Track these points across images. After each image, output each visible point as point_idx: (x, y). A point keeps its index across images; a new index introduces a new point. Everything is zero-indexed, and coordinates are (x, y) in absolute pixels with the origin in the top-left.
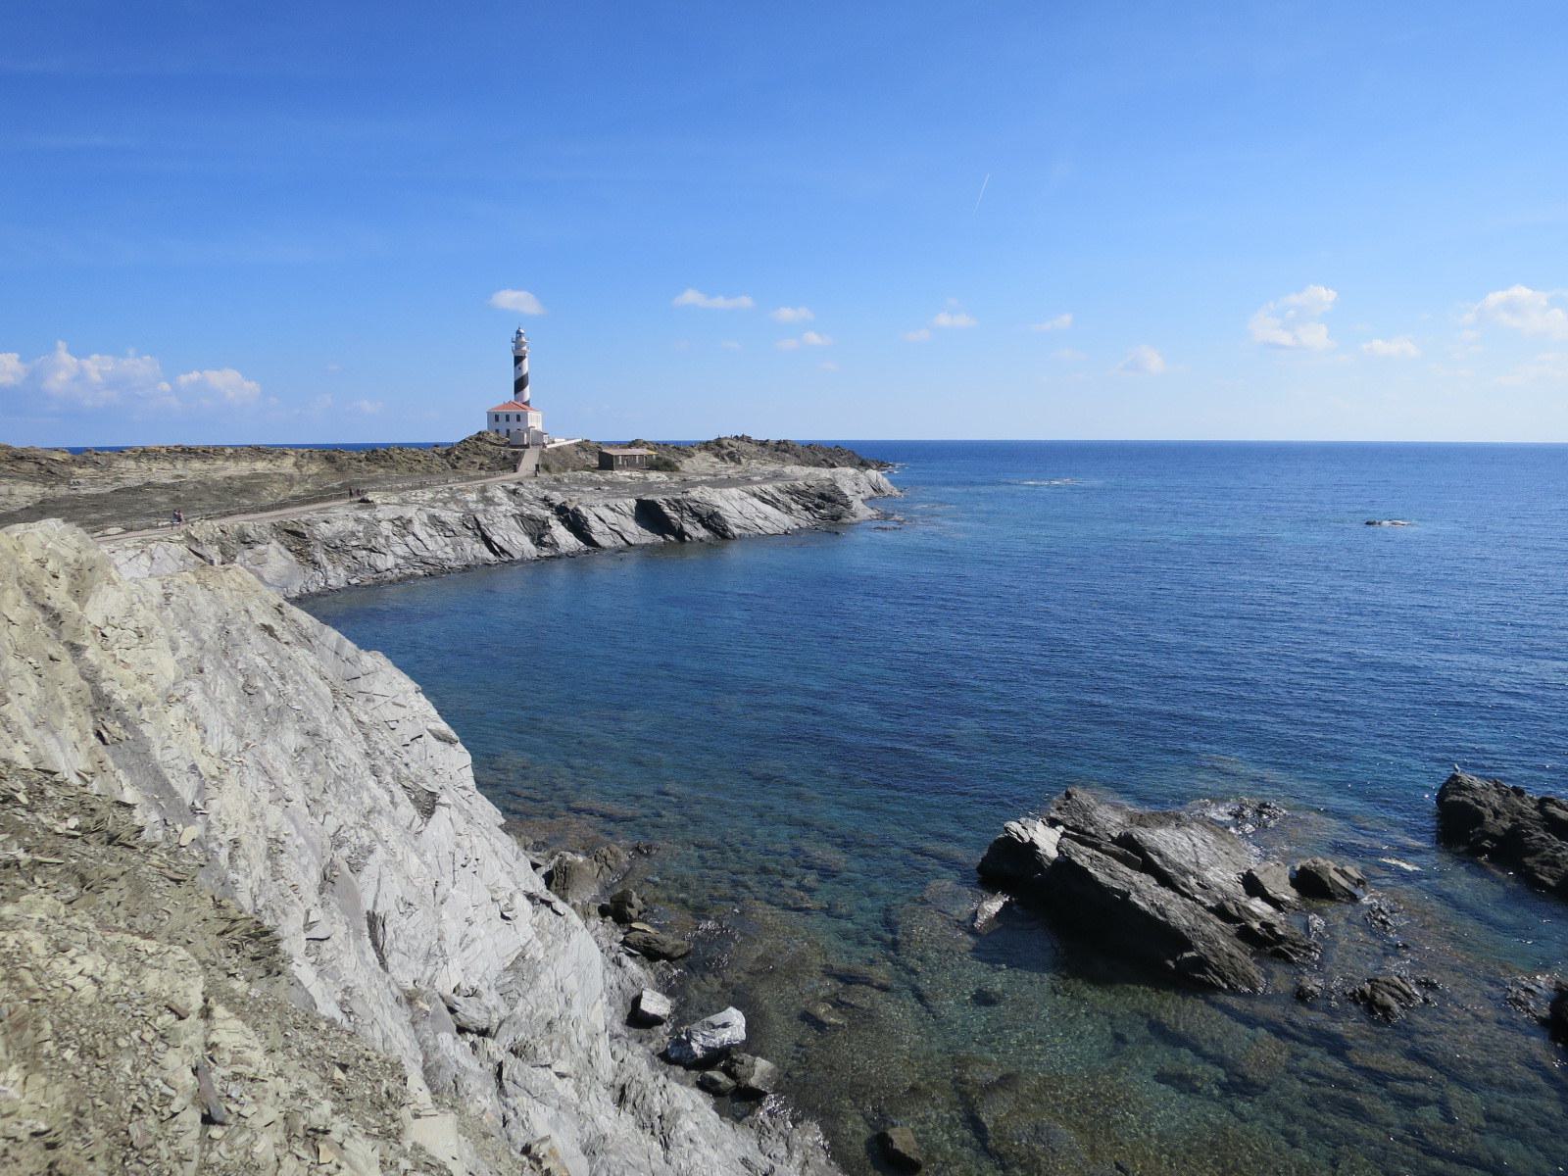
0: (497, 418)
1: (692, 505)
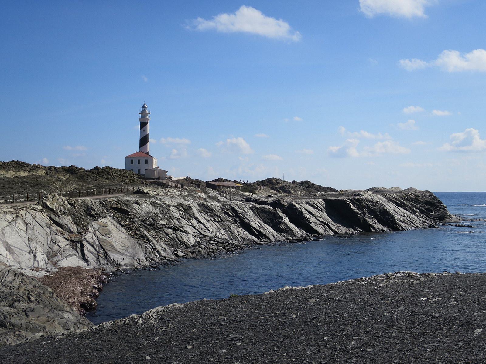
0: (132, 161)
1: (369, 203)
